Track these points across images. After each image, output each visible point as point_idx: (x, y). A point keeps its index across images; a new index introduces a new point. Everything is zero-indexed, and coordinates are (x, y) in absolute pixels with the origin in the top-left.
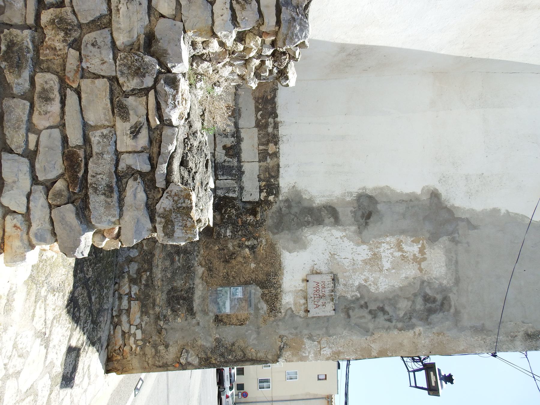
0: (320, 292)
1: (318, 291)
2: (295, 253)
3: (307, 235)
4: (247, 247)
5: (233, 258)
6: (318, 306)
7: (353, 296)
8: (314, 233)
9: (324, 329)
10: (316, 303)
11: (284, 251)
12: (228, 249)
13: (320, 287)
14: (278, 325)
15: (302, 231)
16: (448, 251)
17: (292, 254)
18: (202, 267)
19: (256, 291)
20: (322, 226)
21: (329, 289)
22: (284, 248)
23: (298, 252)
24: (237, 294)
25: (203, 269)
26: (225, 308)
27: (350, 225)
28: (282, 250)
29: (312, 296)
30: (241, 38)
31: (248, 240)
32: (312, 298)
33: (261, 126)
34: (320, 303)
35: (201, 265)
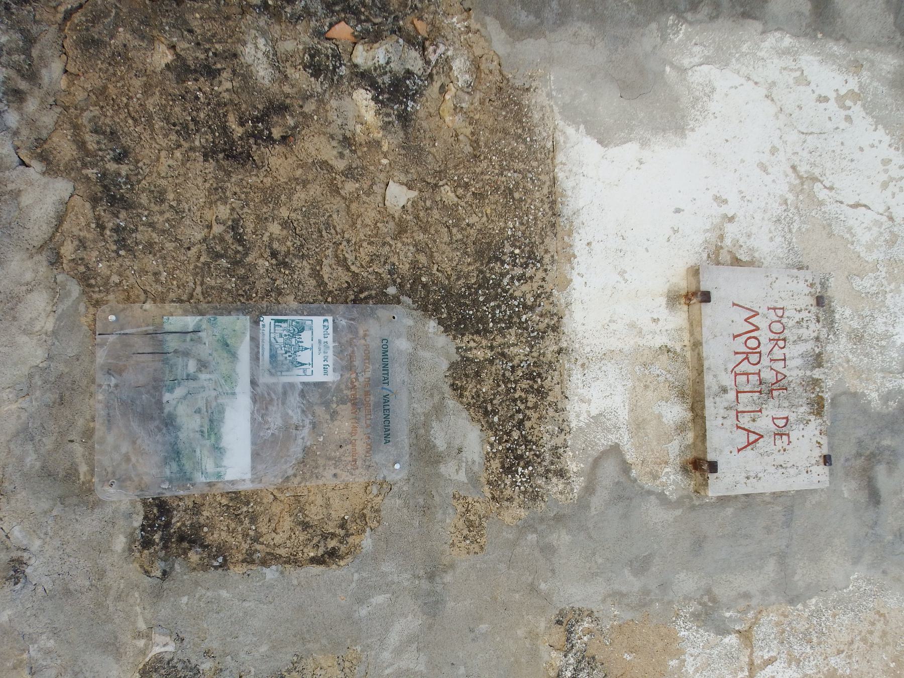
0: (765, 361)
1: (754, 358)
2: (631, 150)
3: (686, 62)
4: (365, 78)
5: (277, 133)
6: (753, 440)
7: (886, 398)
8: (720, 58)
9: (771, 566)
10: (745, 421)
11: (570, 131)
12: (245, 76)
13: (764, 335)
14: (548, 550)
15: (664, 39)
17: (613, 151)
18: (51, 167)
20: (758, 25)
21: (802, 348)
22: (573, 115)
23: (644, 143)
24: (303, 357)
25: (62, 187)
26: (218, 450)
27: (877, 45)
28: (561, 123)
29: (727, 380)
31: (374, 37)
32: (725, 390)
34: (764, 424)
35: (44, 158)
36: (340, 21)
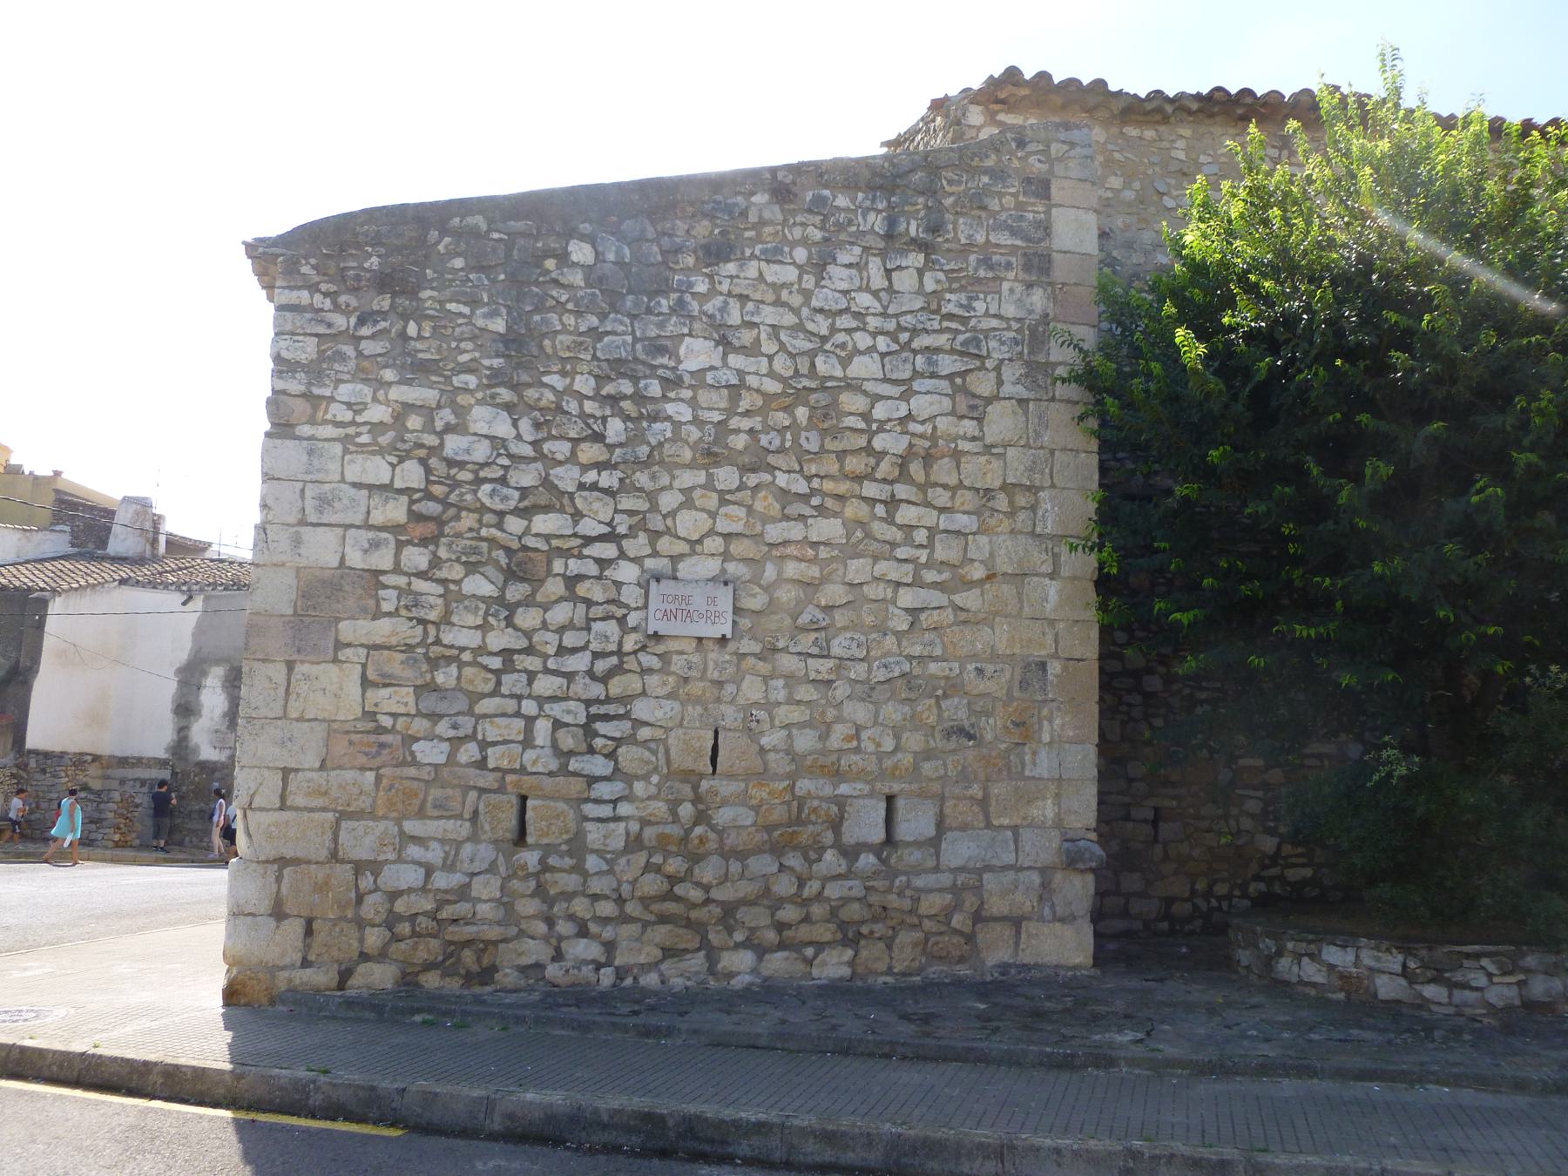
16: (210, 666)
19: (217, 775)
30: (67, 776)
33: (133, 765)
36: (30, 752)
